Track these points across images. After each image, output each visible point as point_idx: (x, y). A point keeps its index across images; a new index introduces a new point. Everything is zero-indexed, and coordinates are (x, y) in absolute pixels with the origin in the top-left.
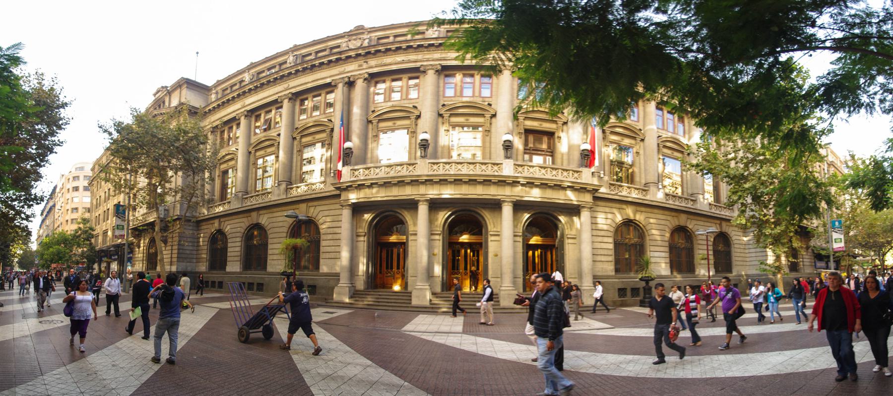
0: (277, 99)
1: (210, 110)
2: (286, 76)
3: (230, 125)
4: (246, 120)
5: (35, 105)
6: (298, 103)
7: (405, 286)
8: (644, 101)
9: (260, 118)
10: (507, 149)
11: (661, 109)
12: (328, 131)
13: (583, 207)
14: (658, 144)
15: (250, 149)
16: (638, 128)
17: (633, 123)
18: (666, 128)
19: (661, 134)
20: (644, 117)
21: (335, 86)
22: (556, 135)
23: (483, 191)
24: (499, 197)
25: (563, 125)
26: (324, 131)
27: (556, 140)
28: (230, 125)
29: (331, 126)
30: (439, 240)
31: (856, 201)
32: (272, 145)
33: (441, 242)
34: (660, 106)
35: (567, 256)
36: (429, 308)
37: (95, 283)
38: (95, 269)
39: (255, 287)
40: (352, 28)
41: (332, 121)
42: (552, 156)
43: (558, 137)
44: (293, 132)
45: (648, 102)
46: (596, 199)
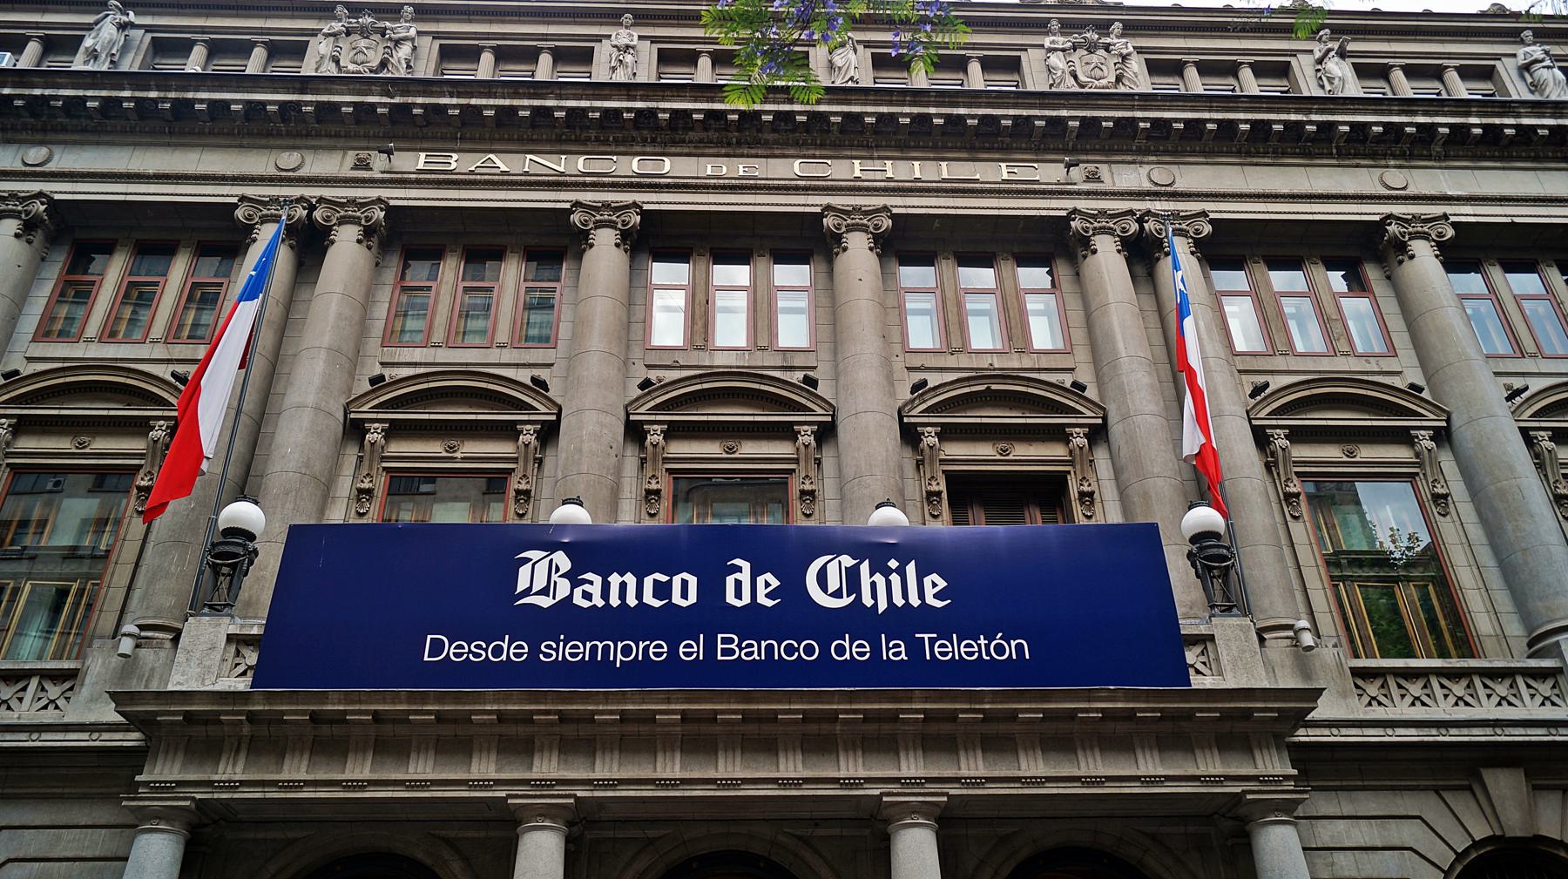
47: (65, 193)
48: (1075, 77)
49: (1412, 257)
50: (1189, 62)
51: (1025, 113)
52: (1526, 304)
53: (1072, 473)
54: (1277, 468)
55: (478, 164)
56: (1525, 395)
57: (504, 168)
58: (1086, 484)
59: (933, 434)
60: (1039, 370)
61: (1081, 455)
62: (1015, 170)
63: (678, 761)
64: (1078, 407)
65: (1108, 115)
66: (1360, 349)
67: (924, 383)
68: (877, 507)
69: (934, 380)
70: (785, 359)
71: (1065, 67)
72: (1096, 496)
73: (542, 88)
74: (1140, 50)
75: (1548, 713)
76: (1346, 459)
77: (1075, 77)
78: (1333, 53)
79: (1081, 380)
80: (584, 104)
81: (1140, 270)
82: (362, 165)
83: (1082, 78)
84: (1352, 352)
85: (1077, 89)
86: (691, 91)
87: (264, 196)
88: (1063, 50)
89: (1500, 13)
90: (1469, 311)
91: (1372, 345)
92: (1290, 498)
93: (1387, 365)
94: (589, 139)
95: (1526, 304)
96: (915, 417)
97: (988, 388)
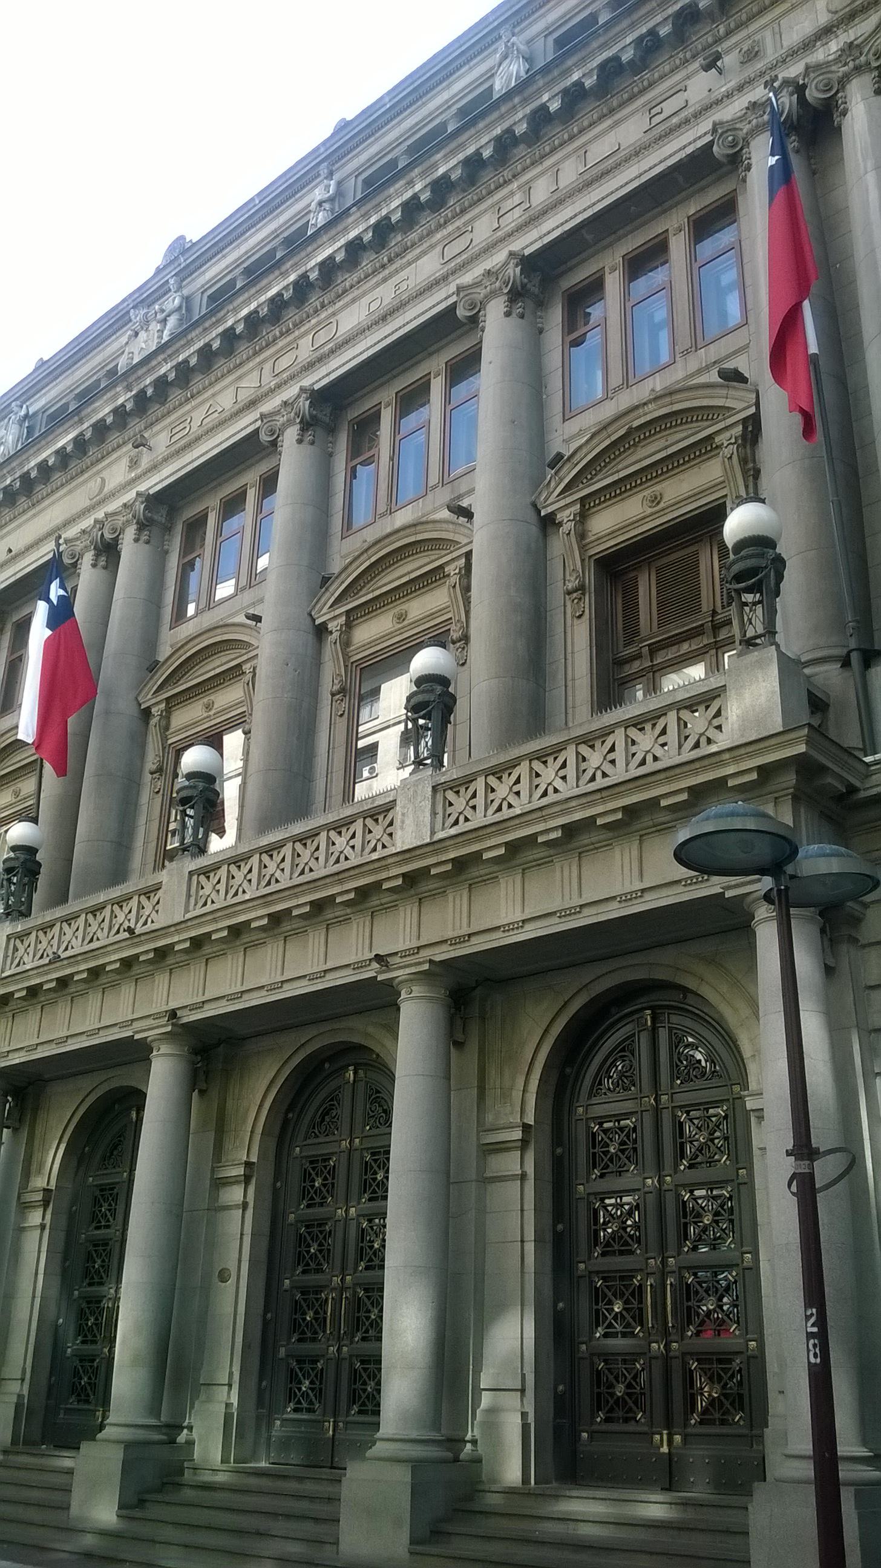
0: (453, 308)
1: (43, 467)
2: (340, 267)
3: (229, 489)
4: (306, 448)
6: (556, 315)
7: (555, 1388)
9: (374, 440)
12: (729, 438)
15: (148, 699)
21: (474, 322)
26: (705, 448)
28: (229, 489)
29: (739, 402)
31: (719, 1142)
32: (434, 577)
37: (700, 1185)
38: (700, 1060)
39: (620, 1335)
40: (332, 131)
41: (744, 380)
44: (537, 483)
86: (326, 233)
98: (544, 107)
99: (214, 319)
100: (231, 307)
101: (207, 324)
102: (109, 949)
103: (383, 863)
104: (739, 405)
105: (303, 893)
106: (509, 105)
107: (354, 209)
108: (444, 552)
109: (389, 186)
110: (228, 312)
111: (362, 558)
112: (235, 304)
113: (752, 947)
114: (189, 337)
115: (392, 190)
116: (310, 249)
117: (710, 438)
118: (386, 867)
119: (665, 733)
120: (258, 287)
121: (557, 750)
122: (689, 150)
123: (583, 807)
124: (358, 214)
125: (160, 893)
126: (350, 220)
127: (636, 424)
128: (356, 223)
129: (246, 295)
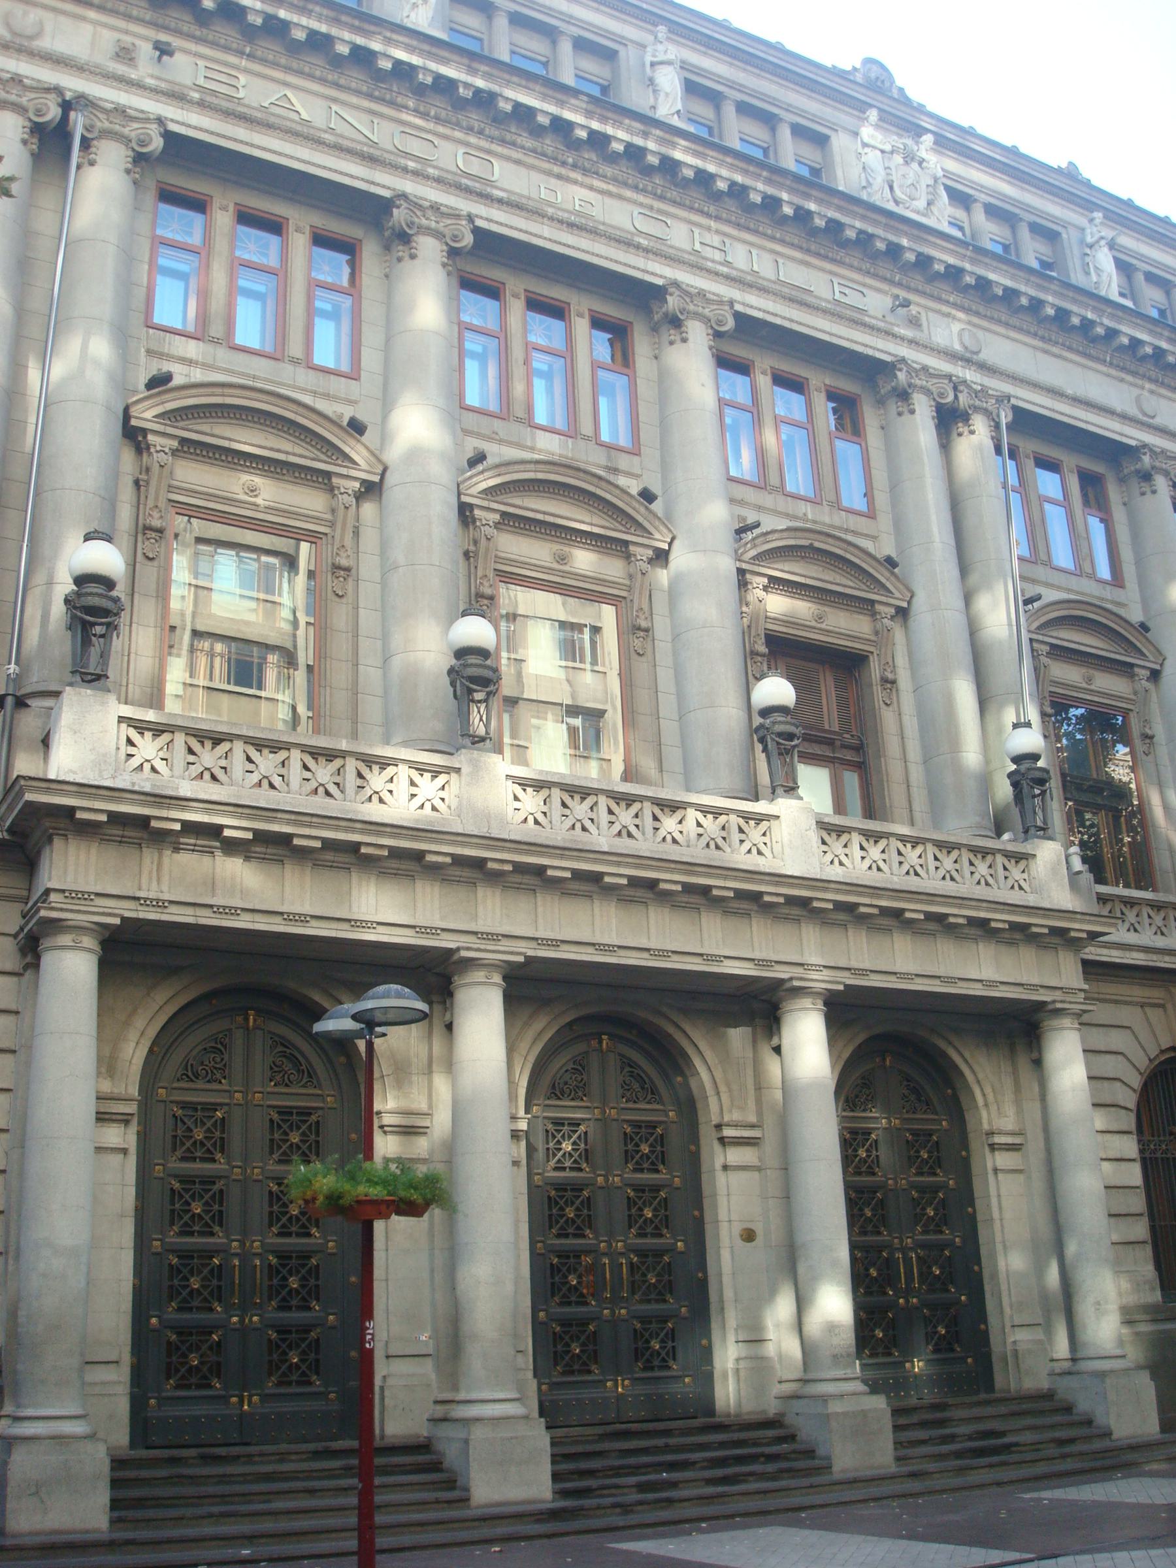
5: (512, 872)
8: (655, 329)
10: (86, 626)
11: (742, 368)
13: (1058, 1012)
14: (741, 572)
16: (880, 555)
17: (854, 522)
18: (1043, 556)
19: (751, 517)
20: (1139, 562)
22: (875, 670)
23: (442, 919)
24: (447, 942)
25: (359, 497)
27: (878, 693)
30: (124, 1151)
33: (132, 1160)
34: (739, 351)
35: (722, 1202)
36: (893, 1477)
42: (861, 767)
43: (885, 681)
45: (674, 335)
46: (1091, 968)
47: (1113, 431)
48: (891, 188)
49: (413, 257)
50: (566, 34)
51: (870, 230)
52: (1047, 506)
53: (329, 537)
54: (476, 561)
55: (272, 100)
56: (756, 532)
57: (305, 116)
58: (344, 555)
59: (491, 524)
60: (847, 530)
61: (160, 475)
62: (847, 291)
63: (865, 940)
64: (888, 585)
65: (854, 225)
66: (605, 437)
67: (1039, 597)
68: (87, 538)
69: (769, 523)
70: (609, 458)
71: (883, 173)
72: (354, 572)
73: (370, 23)
74: (1112, 245)
75: (1160, 942)
76: (1084, 685)
77: (891, 188)
78: (1103, 243)
79: (361, 416)
80: (415, 60)
81: (618, 346)
82: (125, 54)
83: (898, 193)
84: (837, 505)
85: (891, 206)
86: (544, 85)
87: (107, 101)
88: (883, 152)
89: (1071, 173)
90: (728, 420)
91: (798, 485)
92: (753, 653)
93: (862, 524)
94: (1057, 343)
95: (1047, 506)
96: (146, 415)
97: (811, 544)
98: (778, 202)
99: (357, 23)
100: (388, 34)
101: (344, 18)
102: (279, 815)
103: (826, 885)
104: (897, 595)
105: (735, 879)
106: (758, 171)
107: (585, 98)
108: (323, 457)
109: (628, 117)
110: (379, 34)
111: (529, 467)
112: (395, 36)
113: (966, 1080)
114: (310, 6)
115: (627, 121)
116: (515, 79)
117: (1132, 665)
118: (825, 889)
119: (43, 741)
120: (434, 50)
121: (887, 835)
122: (870, 352)
123: (988, 910)
124: (584, 106)
125: (774, 823)
126: (573, 101)
127: (817, 544)
128: (629, 130)
129: (415, 43)
